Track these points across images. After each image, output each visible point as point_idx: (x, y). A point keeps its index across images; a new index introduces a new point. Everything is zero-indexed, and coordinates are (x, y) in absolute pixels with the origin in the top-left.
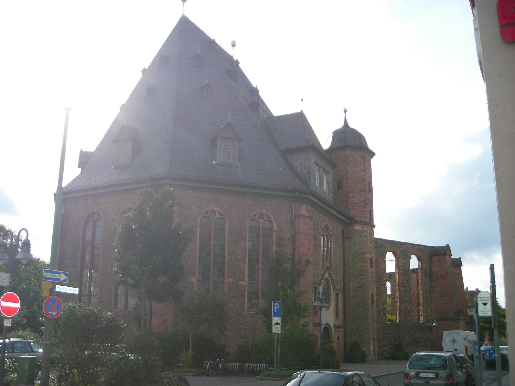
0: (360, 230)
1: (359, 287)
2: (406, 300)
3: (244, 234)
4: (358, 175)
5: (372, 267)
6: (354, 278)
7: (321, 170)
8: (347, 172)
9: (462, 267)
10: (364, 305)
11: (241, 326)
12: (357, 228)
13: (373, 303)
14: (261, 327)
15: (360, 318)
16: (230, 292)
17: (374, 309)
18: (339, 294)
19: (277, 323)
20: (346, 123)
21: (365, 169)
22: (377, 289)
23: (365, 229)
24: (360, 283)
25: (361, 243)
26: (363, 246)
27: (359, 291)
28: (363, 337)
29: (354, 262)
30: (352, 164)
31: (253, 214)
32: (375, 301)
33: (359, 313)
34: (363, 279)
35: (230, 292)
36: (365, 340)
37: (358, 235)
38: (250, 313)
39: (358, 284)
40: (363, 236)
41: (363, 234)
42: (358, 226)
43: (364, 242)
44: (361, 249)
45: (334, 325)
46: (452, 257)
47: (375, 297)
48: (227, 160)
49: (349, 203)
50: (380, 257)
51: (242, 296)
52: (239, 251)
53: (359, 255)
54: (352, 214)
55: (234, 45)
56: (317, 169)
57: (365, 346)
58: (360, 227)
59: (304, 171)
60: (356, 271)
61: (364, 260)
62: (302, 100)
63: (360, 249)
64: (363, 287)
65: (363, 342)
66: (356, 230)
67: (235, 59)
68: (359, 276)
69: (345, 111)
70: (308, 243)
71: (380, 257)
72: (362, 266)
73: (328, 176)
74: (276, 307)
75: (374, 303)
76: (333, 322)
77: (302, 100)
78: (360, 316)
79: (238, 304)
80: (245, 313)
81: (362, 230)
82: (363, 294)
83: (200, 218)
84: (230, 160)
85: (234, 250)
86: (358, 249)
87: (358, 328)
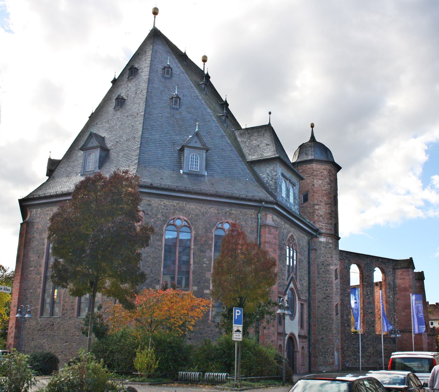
1: (324, 298)
2: (370, 311)
5: (336, 278)
7: (288, 182)
8: (313, 185)
9: (424, 281)
10: (328, 316)
11: (205, 335)
13: (337, 314)
15: (325, 328)
19: (238, 331)
20: (313, 137)
22: (342, 300)
25: (326, 255)
26: (328, 258)
27: (323, 302)
28: (328, 347)
30: (318, 178)
32: (339, 312)
34: (327, 290)
36: (329, 350)
42: (324, 238)
43: (329, 253)
44: (326, 260)
46: (415, 271)
48: (194, 170)
55: (205, 60)
56: (283, 181)
57: (330, 356)
58: (325, 239)
59: (271, 182)
60: (321, 282)
64: (328, 298)
65: (327, 352)
66: (321, 241)
68: (324, 287)
73: (295, 188)
74: (237, 314)
76: (298, 332)
78: (324, 327)
80: (210, 322)
82: (327, 305)
83: (165, 226)
84: (197, 169)
86: (323, 260)
87: (323, 339)
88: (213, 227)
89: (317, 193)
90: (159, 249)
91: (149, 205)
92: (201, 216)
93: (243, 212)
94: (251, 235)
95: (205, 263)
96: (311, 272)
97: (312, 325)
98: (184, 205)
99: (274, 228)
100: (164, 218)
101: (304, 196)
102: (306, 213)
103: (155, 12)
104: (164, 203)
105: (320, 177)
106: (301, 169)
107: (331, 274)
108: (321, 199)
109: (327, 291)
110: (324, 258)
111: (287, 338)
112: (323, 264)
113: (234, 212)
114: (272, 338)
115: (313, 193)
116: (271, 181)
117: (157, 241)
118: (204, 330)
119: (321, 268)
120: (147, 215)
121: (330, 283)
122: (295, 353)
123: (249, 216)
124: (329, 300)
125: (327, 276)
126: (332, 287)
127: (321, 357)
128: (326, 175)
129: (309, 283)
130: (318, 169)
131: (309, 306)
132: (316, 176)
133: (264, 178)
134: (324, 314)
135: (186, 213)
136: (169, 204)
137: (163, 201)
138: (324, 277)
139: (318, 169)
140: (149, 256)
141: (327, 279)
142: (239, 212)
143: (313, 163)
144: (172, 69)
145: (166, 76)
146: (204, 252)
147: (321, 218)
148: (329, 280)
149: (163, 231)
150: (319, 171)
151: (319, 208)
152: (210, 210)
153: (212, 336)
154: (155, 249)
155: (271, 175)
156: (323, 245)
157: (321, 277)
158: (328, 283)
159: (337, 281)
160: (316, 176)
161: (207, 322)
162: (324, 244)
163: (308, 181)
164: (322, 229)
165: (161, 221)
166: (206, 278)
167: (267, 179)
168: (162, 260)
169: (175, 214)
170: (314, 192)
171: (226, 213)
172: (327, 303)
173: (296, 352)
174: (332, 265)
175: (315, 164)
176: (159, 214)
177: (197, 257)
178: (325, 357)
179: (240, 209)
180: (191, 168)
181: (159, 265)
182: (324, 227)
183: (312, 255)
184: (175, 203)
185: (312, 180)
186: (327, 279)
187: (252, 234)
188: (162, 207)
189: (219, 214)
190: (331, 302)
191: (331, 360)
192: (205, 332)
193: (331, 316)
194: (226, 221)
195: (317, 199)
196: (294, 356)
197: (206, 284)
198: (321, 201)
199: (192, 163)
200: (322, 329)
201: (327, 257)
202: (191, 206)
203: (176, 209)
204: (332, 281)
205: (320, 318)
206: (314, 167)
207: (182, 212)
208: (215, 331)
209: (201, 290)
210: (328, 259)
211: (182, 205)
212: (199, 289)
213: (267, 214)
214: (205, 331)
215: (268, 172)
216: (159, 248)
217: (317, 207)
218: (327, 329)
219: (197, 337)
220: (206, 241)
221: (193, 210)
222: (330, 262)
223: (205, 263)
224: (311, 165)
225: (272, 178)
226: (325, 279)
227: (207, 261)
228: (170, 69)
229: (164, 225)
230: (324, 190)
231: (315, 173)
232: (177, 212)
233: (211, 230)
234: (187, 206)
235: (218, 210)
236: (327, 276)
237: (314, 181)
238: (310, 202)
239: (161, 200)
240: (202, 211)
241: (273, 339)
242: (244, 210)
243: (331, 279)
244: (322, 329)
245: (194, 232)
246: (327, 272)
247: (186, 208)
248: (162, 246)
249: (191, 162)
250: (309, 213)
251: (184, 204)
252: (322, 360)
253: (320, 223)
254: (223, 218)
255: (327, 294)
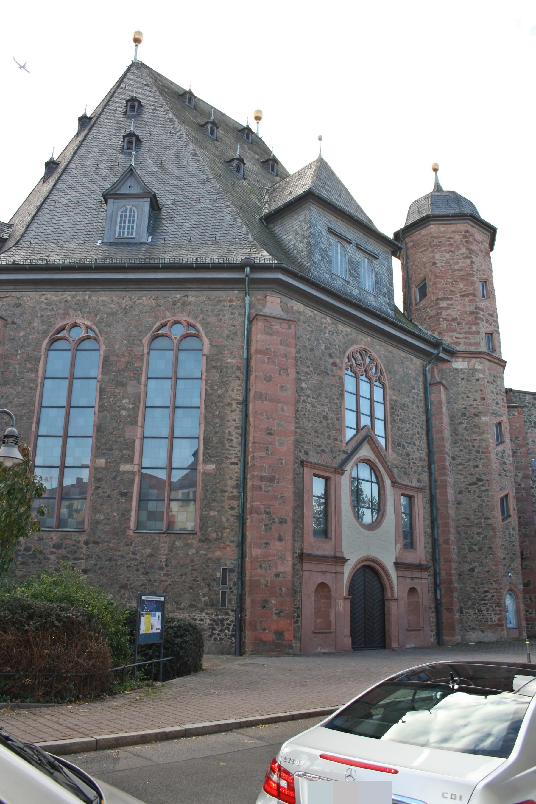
0: (466, 369)
1: (470, 485)
3: (135, 365)
4: (456, 267)
6: (459, 465)
8: (434, 264)
10: (482, 521)
11: (119, 563)
12: (459, 364)
14: (167, 565)
15: (475, 548)
16: (99, 487)
17: (513, 529)
18: (413, 496)
20: (438, 187)
21: (470, 253)
23: (478, 367)
24: (472, 474)
25: (470, 395)
26: (475, 400)
27: (470, 492)
28: (486, 589)
29: (457, 433)
30: (443, 249)
31: (158, 324)
33: (472, 538)
34: (477, 466)
35: (99, 487)
36: (489, 596)
37: (463, 379)
38: (142, 533)
39: (467, 477)
40: (474, 381)
41: (473, 376)
42: (463, 361)
43: (476, 392)
44: (471, 405)
45: (396, 564)
47: (512, 504)
49: (441, 320)
50: (531, 429)
51: (124, 494)
52: (124, 402)
53: (466, 419)
54: (447, 340)
55: (258, 118)
57: (491, 608)
58: (466, 363)
59: (301, 245)
60: (461, 450)
61: (479, 429)
62: (320, 139)
63: (468, 407)
64: (480, 483)
65: (485, 600)
66: (456, 369)
67: (260, 136)
68: (469, 460)
69: (435, 170)
70: (280, 374)
71: (531, 429)
72: (476, 439)
75: (510, 516)
76: (394, 557)
77: (320, 139)
78: (476, 545)
79: (115, 514)
80: (131, 533)
81: (471, 370)
82: (479, 497)
85: (113, 401)
86: (464, 406)
87: (472, 570)
88: (146, 334)
89: (442, 277)
90: (31, 388)
91: (18, 306)
92: (122, 315)
93: (212, 298)
94: (231, 342)
95: (125, 409)
96: (434, 430)
97: (441, 541)
98: (87, 297)
99: (280, 321)
100: (44, 327)
101: (419, 289)
102: (425, 319)
103: (137, 41)
104: (46, 299)
105: (448, 248)
106: (411, 242)
107: (483, 433)
108: (451, 288)
109: (476, 469)
110: (465, 401)
111: (348, 570)
112: (464, 415)
113: (193, 299)
114: (276, 567)
115: (435, 279)
116: (301, 242)
117: (28, 372)
118: (119, 551)
119: (460, 423)
120: (13, 325)
121: (483, 452)
122: (386, 603)
123: (225, 304)
124: (483, 488)
125: (474, 437)
126: (489, 459)
127: (471, 612)
128: (458, 243)
129: (430, 453)
130: (442, 233)
131: (432, 500)
132: (439, 246)
133: (290, 241)
134: (472, 516)
135: (90, 313)
136: (55, 299)
137: (44, 295)
138: (467, 441)
139: (442, 233)
140: (10, 402)
141: (476, 444)
142: (203, 298)
143: (430, 225)
144: (139, 102)
145: (129, 113)
146: (124, 385)
147: (454, 324)
148: (479, 447)
149: (40, 352)
150: (442, 237)
151: (448, 304)
152: (140, 301)
153: (137, 565)
154: (23, 388)
155: (300, 232)
156: (462, 376)
157: (462, 440)
158: (478, 452)
159: (501, 448)
160: (439, 246)
161: (125, 533)
162: (463, 373)
163: (425, 259)
164: (458, 344)
165: (39, 333)
166: (125, 440)
167: (295, 241)
168: (34, 410)
169: (67, 317)
170: (436, 277)
171: (174, 304)
172: (477, 494)
173: (389, 600)
174: (485, 416)
175: (435, 225)
176: (36, 319)
177: (109, 397)
178: (480, 611)
179: (206, 293)
180: (119, 234)
181: (28, 419)
182: (462, 341)
183: (433, 395)
184: (69, 295)
185: (431, 255)
186: (475, 444)
187: (232, 339)
188: (43, 306)
189: (159, 306)
190: (487, 490)
191: (495, 618)
192: (122, 557)
193: (489, 521)
194: (175, 318)
195: (444, 288)
196: (386, 608)
197: (124, 452)
198: (451, 291)
199: (122, 225)
200: (471, 550)
201: (472, 398)
202: (100, 299)
203: (70, 307)
204: (487, 447)
205: (462, 525)
206: (432, 230)
207: (80, 310)
208: (142, 554)
209: (113, 464)
210: (474, 403)
211: (81, 299)
212: (110, 462)
213: (266, 297)
214: (119, 553)
215: (297, 227)
216: (31, 385)
217: (443, 304)
218: (480, 549)
219: (101, 568)
220: (128, 363)
221: (104, 305)
222: (481, 408)
223: (125, 409)
224: (428, 228)
225: (303, 237)
226: (470, 444)
227: (130, 402)
228: (136, 104)
229: (44, 339)
230: (456, 270)
231: (436, 241)
232: (71, 313)
233: (141, 341)
234: (93, 298)
235: (157, 299)
236: (474, 437)
237: (434, 257)
238: (431, 296)
239: (42, 293)
240: (123, 306)
241: (281, 569)
242: (215, 293)
243: (484, 444)
244: (471, 550)
245: (103, 348)
246: (475, 429)
247: (90, 302)
248: (37, 380)
249: (121, 223)
250: (429, 318)
251: (86, 295)
252: (474, 616)
253: (452, 334)
254: (168, 314)
255: (477, 476)
